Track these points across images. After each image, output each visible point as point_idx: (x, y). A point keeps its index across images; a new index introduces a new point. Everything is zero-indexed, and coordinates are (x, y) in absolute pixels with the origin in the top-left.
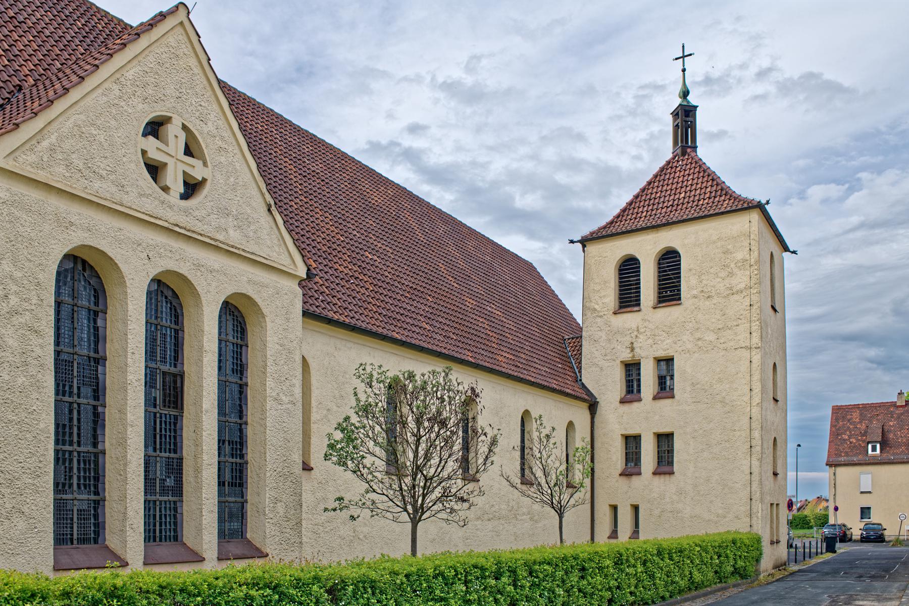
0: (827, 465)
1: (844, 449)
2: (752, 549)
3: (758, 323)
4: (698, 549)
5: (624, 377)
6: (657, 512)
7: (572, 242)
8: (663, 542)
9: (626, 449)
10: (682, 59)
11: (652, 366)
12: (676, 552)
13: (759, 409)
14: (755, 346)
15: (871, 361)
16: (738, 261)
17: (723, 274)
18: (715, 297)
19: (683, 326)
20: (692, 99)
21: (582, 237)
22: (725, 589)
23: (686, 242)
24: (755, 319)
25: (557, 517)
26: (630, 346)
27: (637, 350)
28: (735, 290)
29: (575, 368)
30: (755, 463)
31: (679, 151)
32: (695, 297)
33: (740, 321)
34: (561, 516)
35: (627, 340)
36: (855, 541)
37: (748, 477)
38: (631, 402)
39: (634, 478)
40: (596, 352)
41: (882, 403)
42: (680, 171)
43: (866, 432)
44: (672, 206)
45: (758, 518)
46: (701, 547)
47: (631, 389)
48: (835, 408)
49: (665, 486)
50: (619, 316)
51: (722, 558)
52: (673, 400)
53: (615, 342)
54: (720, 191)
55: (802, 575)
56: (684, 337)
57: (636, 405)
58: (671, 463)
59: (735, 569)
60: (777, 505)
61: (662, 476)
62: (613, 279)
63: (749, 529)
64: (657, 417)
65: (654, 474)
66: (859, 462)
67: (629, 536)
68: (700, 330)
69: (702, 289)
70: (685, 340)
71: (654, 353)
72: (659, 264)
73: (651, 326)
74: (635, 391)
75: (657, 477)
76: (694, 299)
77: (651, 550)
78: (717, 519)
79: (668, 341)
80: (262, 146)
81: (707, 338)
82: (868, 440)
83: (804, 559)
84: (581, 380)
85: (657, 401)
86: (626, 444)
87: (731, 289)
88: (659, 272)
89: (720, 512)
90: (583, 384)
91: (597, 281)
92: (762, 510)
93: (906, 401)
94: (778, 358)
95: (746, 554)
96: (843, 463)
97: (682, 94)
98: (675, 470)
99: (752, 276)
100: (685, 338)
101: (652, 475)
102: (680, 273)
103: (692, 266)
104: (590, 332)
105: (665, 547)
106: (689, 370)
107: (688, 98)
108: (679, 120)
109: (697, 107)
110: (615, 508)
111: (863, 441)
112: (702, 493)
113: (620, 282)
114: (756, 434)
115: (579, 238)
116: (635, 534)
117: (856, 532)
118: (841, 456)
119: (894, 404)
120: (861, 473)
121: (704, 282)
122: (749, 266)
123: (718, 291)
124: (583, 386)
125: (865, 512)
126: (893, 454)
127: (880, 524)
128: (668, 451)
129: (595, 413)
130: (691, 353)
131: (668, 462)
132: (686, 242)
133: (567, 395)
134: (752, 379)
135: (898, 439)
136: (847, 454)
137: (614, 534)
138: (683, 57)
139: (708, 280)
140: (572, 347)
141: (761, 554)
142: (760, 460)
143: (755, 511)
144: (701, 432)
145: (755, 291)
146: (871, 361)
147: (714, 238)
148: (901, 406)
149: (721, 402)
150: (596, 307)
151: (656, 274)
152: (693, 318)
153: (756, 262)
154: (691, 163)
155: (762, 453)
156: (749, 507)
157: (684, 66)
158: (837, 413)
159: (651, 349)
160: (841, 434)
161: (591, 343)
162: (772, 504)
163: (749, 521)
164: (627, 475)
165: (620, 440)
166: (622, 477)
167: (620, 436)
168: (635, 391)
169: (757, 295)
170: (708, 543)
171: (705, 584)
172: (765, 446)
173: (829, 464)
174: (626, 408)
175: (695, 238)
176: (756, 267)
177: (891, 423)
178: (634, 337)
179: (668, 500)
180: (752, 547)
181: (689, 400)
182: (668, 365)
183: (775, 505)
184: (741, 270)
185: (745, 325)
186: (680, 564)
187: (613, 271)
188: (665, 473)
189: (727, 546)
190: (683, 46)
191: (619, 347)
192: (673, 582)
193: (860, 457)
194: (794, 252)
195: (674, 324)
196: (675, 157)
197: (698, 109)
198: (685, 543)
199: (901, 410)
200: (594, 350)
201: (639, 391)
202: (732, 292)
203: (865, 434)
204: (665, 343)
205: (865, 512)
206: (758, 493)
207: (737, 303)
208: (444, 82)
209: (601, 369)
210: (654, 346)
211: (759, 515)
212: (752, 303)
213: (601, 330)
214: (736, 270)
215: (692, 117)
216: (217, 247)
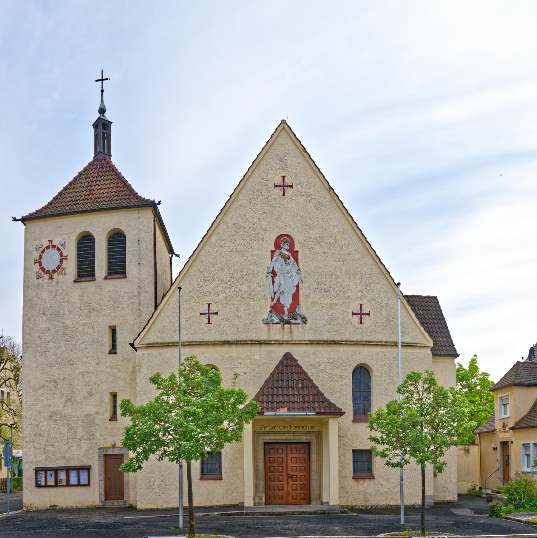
7: (15, 219)
10: (101, 82)
20: (108, 116)
21: (22, 217)
108: (98, 131)
109: (112, 123)
115: (21, 218)
157: (102, 88)
197: (112, 124)
216: (377, 345)
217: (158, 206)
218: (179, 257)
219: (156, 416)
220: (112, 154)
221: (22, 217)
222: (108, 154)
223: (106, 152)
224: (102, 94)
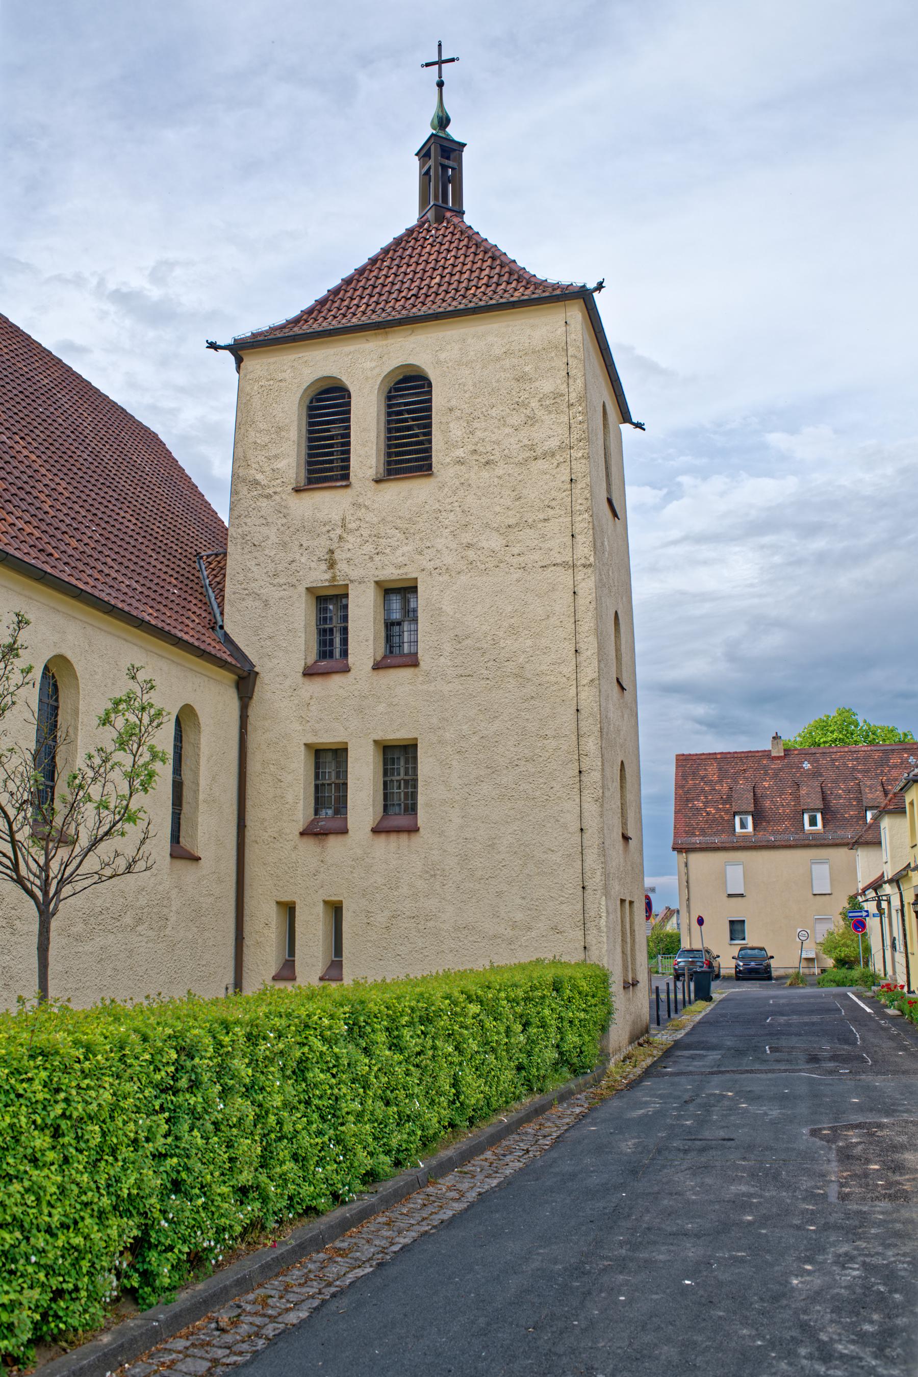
0: (674, 849)
1: (698, 824)
2: (593, 1001)
3: (586, 516)
4: (474, 1008)
5: (314, 623)
6: (381, 918)
7: (213, 346)
8: (374, 995)
10: (437, 66)
11: (372, 598)
12: (411, 1024)
13: (594, 691)
14: (583, 561)
15: (700, 722)
16: (545, 397)
17: (516, 419)
18: (501, 464)
19: (437, 518)
20: (454, 132)
22: (539, 1111)
23: (443, 356)
24: (582, 508)
25: (30, 910)
26: (327, 557)
27: (342, 566)
28: (539, 452)
29: (213, 599)
30: (591, 808)
31: (430, 215)
32: (460, 462)
33: (551, 512)
34: (45, 915)
35: (321, 545)
36: (727, 978)
37: (577, 838)
39: (333, 842)
40: (254, 569)
41: (750, 752)
42: (432, 246)
43: (729, 797)
44: (416, 296)
45: (599, 929)
46: (481, 1003)
47: (328, 648)
48: (682, 758)
49: (399, 858)
50: (305, 495)
51: (533, 1030)
52: (416, 670)
53: (296, 548)
54: (507, 275)
55: (693, 1057)
56: (438, 540)
57: (337, 680)
59: (561, 1053)
60: (631, 903)
61: (393, 837)
62: (296, 423)
63: (582, 956)
64: (381, 708)
65: (376, 831)
66: (724, 845)
67: (320, 974)
68: (470, 527)
69: (473, 447)
70: (440, 547)
71: (377, 573)
72: (389, 398)
73: (371, 517)
75: (382, 838)
76: (458, 467)
77: (326, 1022)
78: (511, 933)
79: (406, 549)
81: (484, 544)
82: (734, 809)
83: (669, 1016)
84: (222, 627)
85: (382, 673)
86: (317, 766)
87: (532, 448)
88: (389, 414)
89: (519, 916)
90: (226, 635)
91: (262, 426)
92: (607, 912)
93: (785, 750)
94: (621, 606)
95: (582, 1015)
96: (698, 846)
97: (436, 122)
98: (420, 823)
99: (573, 426)
100: (440, 543)
101: (370, 834)
102: (430, 417)
103: (454, 403)
104: (246, 529)
105: (375, 1009)
106: (448, 608)
107: (448, 130)
108: (431, 163)
109: (464, 145)
110: (289, 910)
111: (727, 812)
112: (479, 873)
113: (310, 432)
114: (591, 745)
115: (229, 341)
116: (334, 971)
117: (727, 963)
118: (694, 835)
119: (767, 754)
120: (727, 863)
121: (479, 434)
122: (566, 405)
123: (507, 451)
125: (736, 928)
126: (773, 833)
127: (762, 949)
128: (406, 782)
129: (251, 698)
130: (453, 574)
131: (406, 806)
132: (443, 356)
133: (178, 642)
134: (579, 629)
135: (778, 808)
136: (703, 833)
137: (287, 972)
138: (440, 63)
139: (485, 430)
140: (213, 570)
141: (609, 1013)
142: (601, 801)
143: (592, 914)
144: (475, 739)
146: (700, 722)
147: (498, 351)
148: (778, 758)
149: (516, 675)
150: (259, 477)
151: (383, 418)
152: (456, 504)
153: (580, 399)
154: (453, 234)
155: (603, 787)
156: (579, 906)
158: (685, 766)
159: (370, 565)
160: (692, 800)
161: (246, 550)
162: (623, 901)
163: (582, 938)
164: (316, 834)
165: (303, 757)
166: (305, 839)
167: (303, 748)
169: (583, 461)
170: (499, 991)
171: (495, 1105)
172: (608, 774)
173: (678, 849)
174: (316, 686)
175: (461, 349)
176: (580, 409)
177: (766, 784)
178: (336, 539)
179: (405, 890)
180: (593, 996)
181: (449, 672)
182: (405, 602)
183: (627, 904)
184: (550, 412)
185: (561, 520)
186: (425, 1060)
187: (295, 407)
188: (398, 831)
189: (543, 997)
190: (440, 45)
191: (303, 560)
192: (402, 1119)
193: (724, 837)
194: (639, 426)
195: (419, 514)
196: (424, 223)
197: (465, 149)
198: (439, 995)
199: (777, 765)
200: (251, 564)
201: (345, 653)
202: (533, 453)
203: (728, 800)
204: (399, 552)
205: (736, 928)
206: (599, 873)
207: (544, 477)
208: (117, 291)
209: (266, 603)
210: (377, 558)
211: (603, 922)
212: (573, 477)
213: (267, 524)
214: (540, 413)
215: (454, 161)
217: (596, 295)
218: (644, 429)
219: (63, 1191)
222: (455, 208)
224: (440, 77)
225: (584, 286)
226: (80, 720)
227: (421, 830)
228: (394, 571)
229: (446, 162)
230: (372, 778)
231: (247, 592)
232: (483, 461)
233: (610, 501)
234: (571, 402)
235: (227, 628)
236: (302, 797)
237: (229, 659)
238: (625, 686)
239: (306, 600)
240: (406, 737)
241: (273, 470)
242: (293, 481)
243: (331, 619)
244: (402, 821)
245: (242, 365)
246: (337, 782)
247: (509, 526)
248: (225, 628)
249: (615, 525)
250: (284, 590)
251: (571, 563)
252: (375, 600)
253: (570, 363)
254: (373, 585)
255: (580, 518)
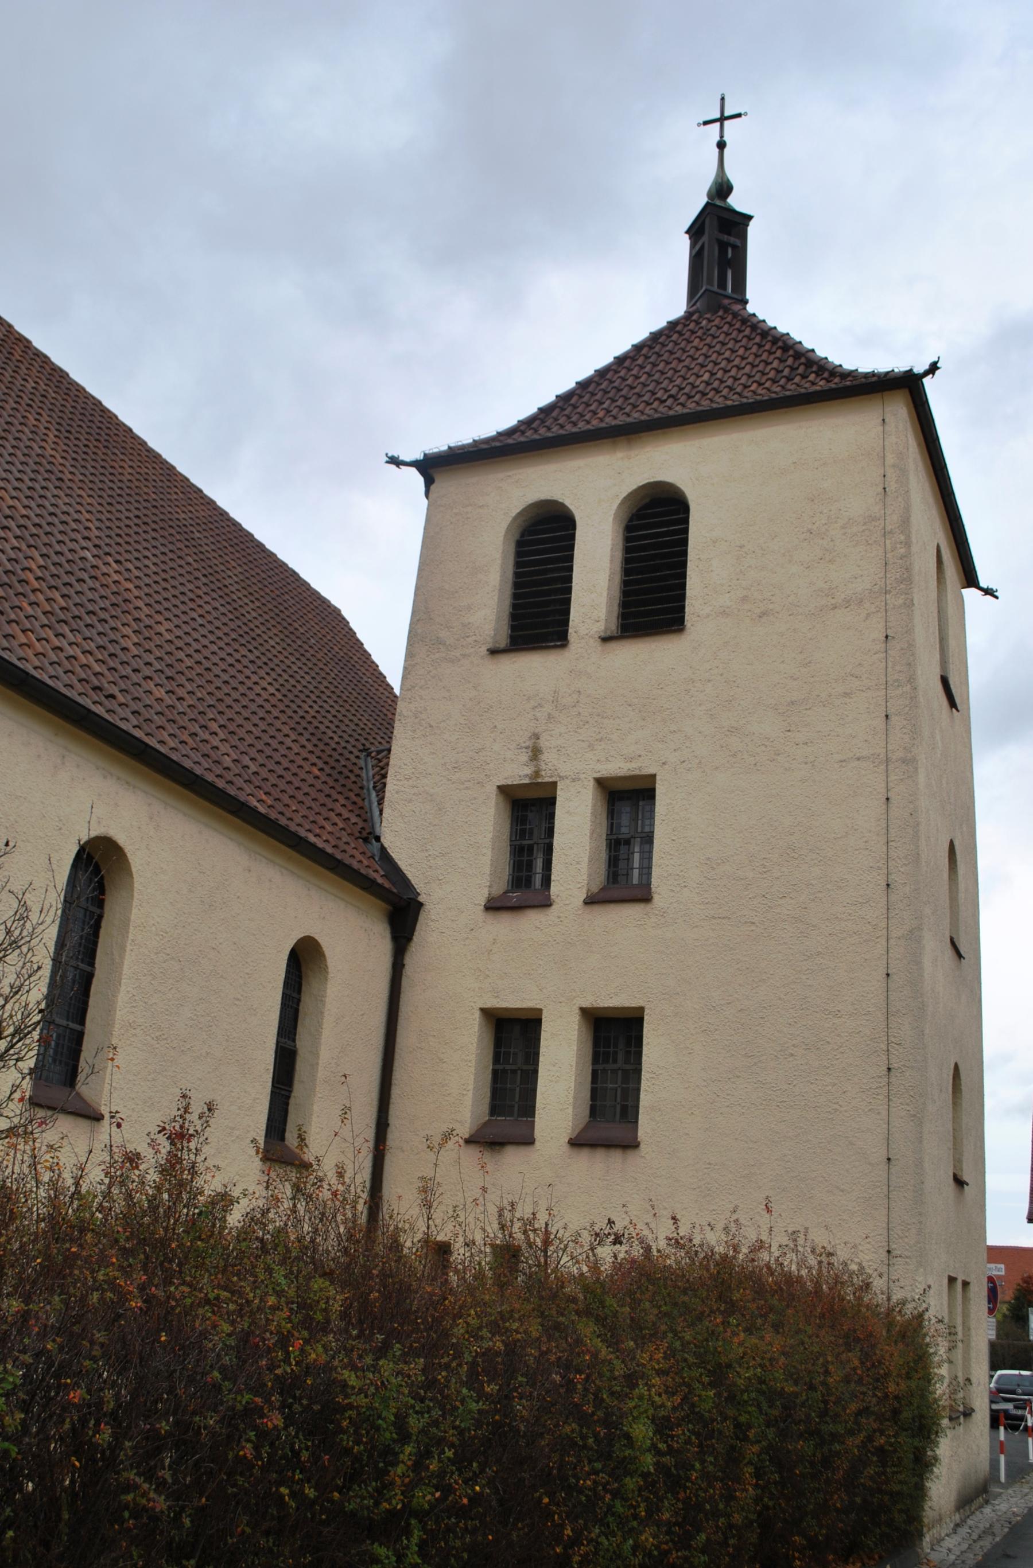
7: (395, 461)
9: (496, 1059)
19: (688, 691)
20: (736, 201)
21: (425, 455)
32: (724, 613)
38: (516, 908)
58: (629, 1112)
60: (966, 1284)
61: (600, 1154)
74: (538, 879)
75: (585, 1154)
80: (37, 624)
84: (378, 839)
85: (597, 909)
101: (566, 1148)
108: (705, 239)
115: (419, 456)
124: (385, 856)
138: (722, 119)
145: (901, 601)
162: (952, 1280)
165: (476, 1029)
167: (477, 1014)
168: (538, 879)
174: (504, 926)
183: (959, 1285)
188: (609, 1145)
190: (723, 99)
194: (989, 592)
197: (752, 223)
201: (547, 881)
218: (997, 597)
220: (748, 297)
221: (425, 455)
222: (735, 296)
223: (730, 290)
224: (722, 136)
225: (911, 370)
226: (131, 937)
227: (642, 1146)
228: (622, 765)
229: (725, 238)
230: (574, 1063)
231: (415, 790)
232: (758, 611)
233: (945, 682)
234: (888, 528)
235: (386, 841)
236: (471, 1087)
237: (380, 880)
238: (962, 953)
239: (497, 804)
240: (627, 1005)
241: (464, 625)
242: (489, 639)
243: (531, 833)
244: (616, 1131)
245: (433, 487)
246: (525, 1067)
247: (793, 703)
248: (382, 839)
249: (952, 717)
250: (467, 788)
251: (883, 756)
252: (594, 806)
253: (888, 475)
254: (591, 784)
255: (899, 691)
